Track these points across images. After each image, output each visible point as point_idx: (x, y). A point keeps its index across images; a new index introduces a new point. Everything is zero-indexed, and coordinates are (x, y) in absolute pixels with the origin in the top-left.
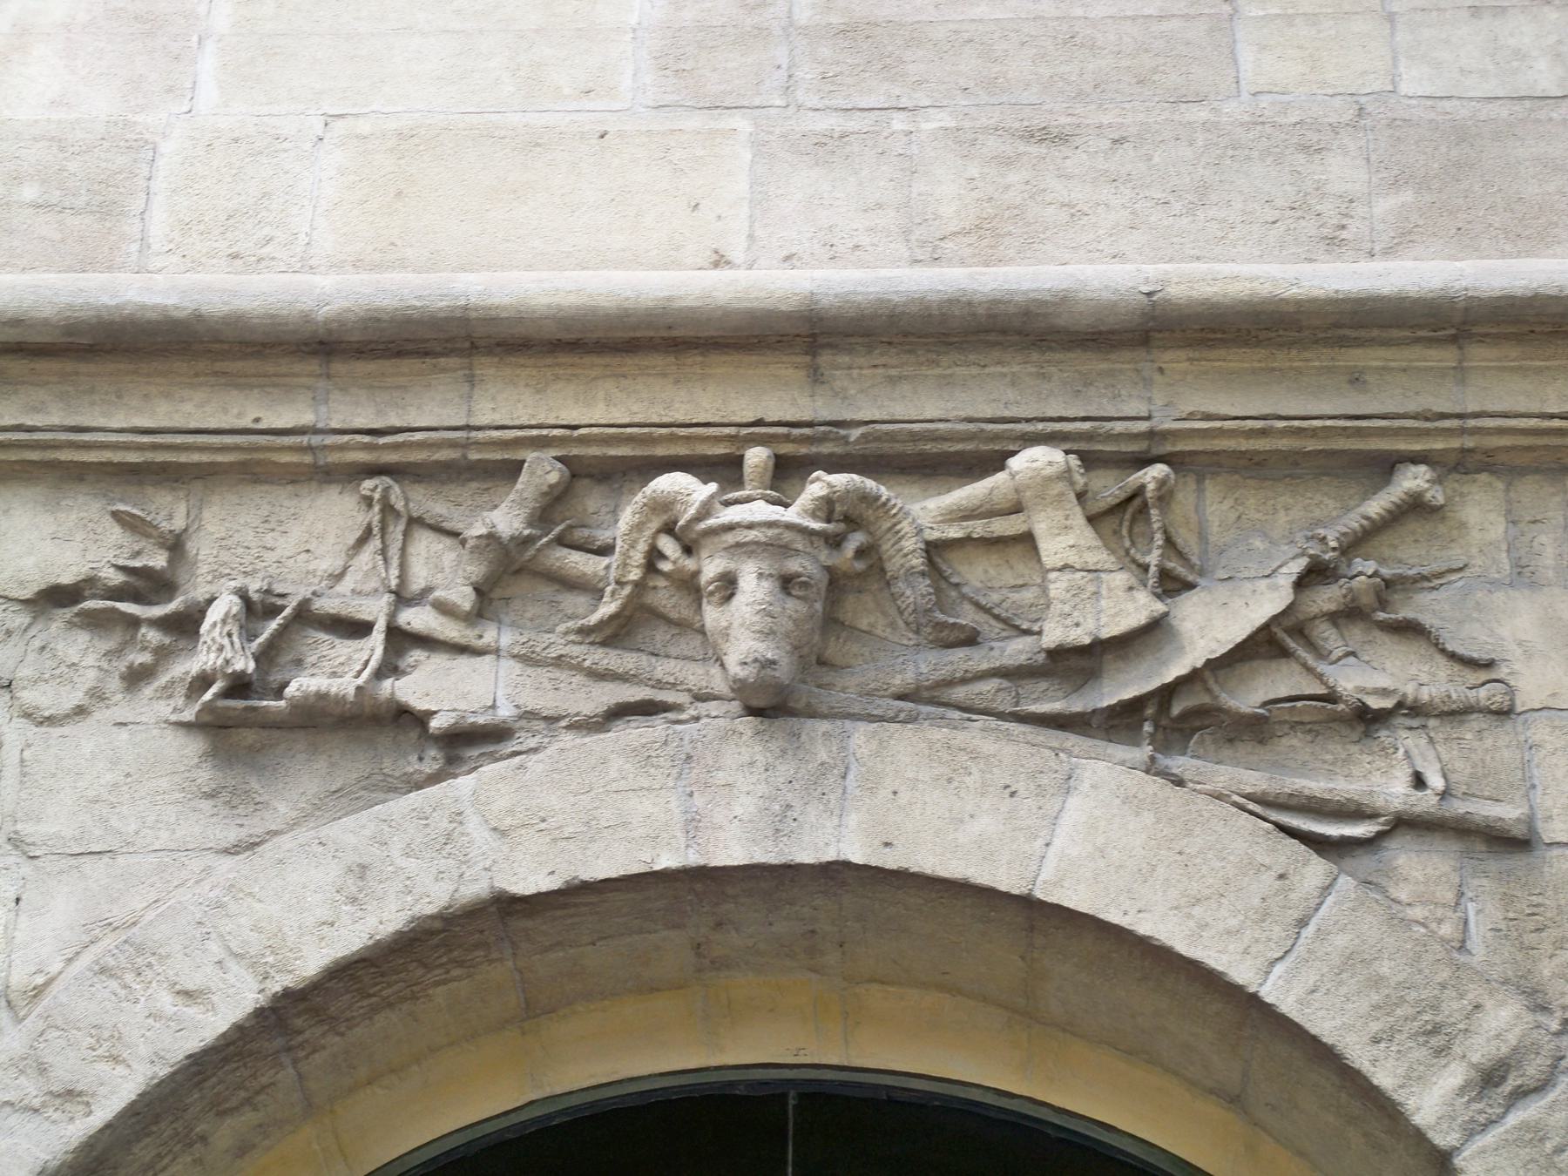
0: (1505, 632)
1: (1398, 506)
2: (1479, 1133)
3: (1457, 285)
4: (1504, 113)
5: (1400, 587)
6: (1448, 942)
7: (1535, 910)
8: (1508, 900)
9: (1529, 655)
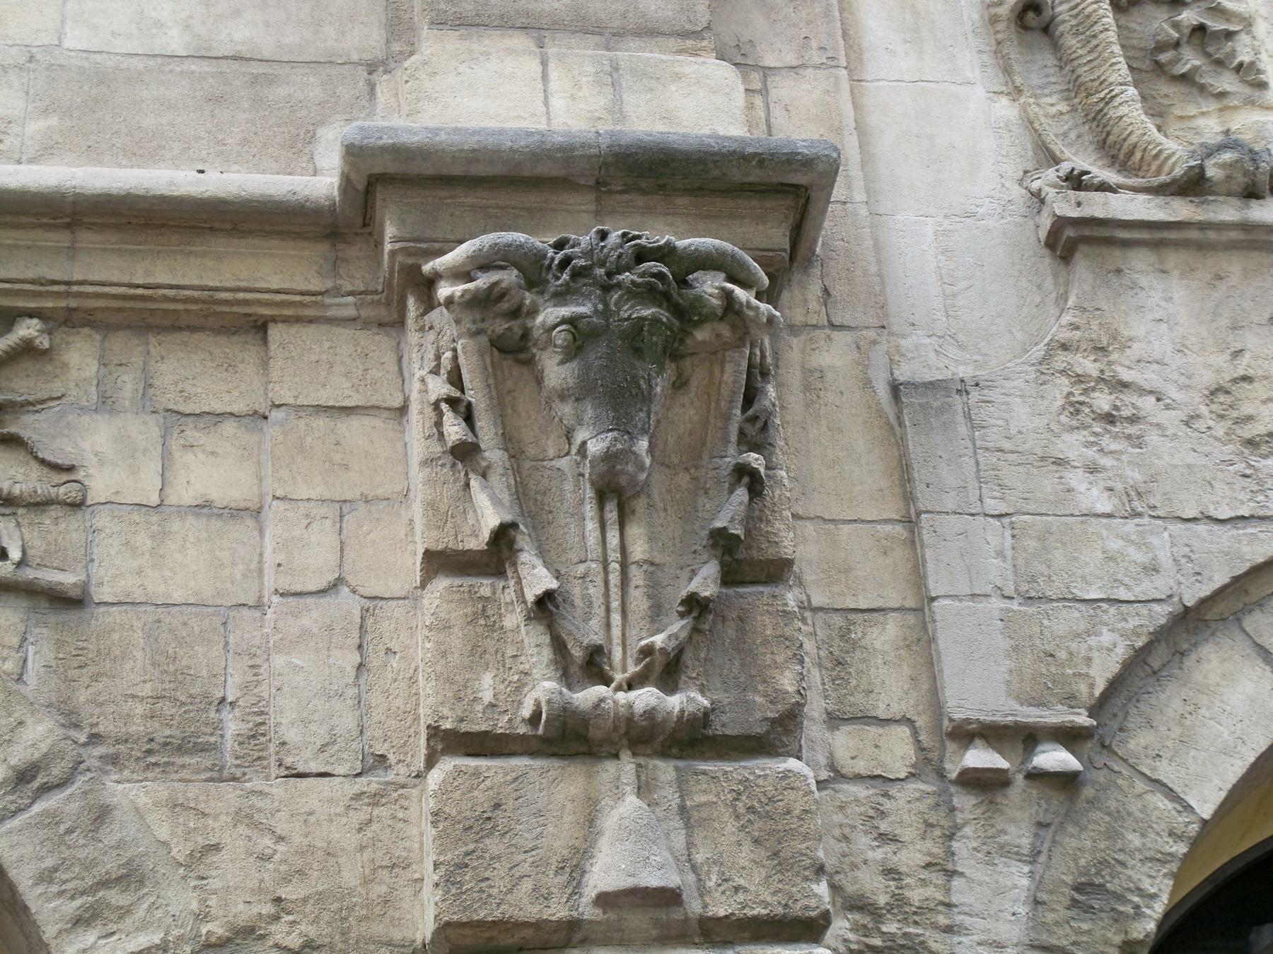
0: (86, 445)
1: (13, 349)
2: (9, 818)
3: (68, 184)
4: (141, 66)
5: (10, 410)
6: (9, 675)
7: (81, 652)
8: (60, 644)
9: (101, 462)
